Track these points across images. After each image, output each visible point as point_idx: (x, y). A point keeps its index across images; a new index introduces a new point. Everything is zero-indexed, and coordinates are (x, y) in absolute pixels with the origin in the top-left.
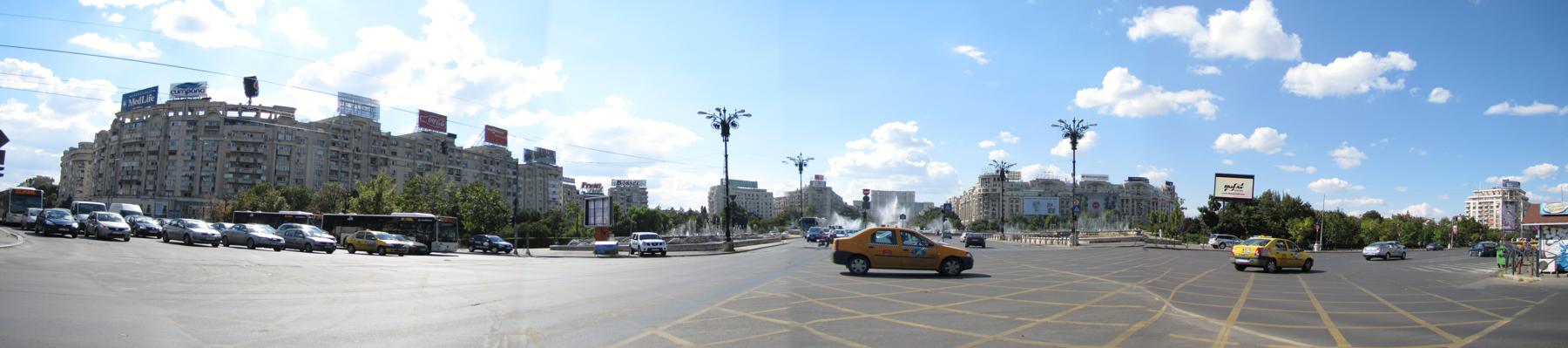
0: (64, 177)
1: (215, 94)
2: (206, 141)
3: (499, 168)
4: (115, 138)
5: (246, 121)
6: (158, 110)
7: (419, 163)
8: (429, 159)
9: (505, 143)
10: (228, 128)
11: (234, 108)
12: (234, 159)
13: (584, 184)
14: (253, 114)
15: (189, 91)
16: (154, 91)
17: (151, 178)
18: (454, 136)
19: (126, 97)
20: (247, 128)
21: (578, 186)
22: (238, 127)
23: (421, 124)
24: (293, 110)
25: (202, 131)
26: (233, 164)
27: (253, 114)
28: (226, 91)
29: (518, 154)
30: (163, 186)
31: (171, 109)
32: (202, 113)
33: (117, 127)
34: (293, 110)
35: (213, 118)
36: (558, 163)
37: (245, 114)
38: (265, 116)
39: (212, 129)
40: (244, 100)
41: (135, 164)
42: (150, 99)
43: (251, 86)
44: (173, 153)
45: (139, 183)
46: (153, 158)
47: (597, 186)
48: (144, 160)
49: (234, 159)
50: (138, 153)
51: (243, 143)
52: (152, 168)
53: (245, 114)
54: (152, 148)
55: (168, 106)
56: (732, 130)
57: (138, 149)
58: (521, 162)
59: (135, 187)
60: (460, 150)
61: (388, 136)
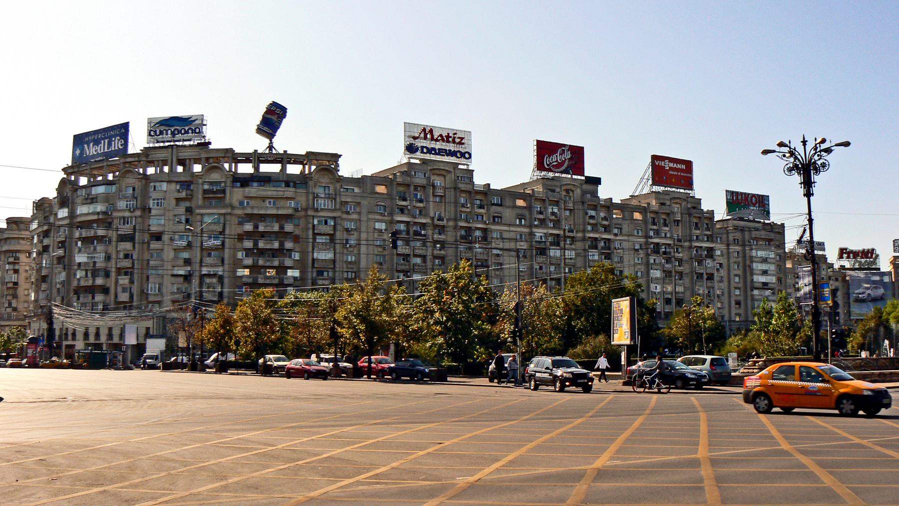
0: (614, 345)
1: (218, 137)
2: (209, 217)
3: (679, 232)
4: (63, 213)
5: (267, 179)
6: (129, 163)
7: (539, 233)
8: (557, 224)
9: (689, 184)
10: (237, 195)
11: (247, 158)
12: (248, 244)
13: (843, 252)
14: (275, 168)
15: (176, 126)
16: (123, 130)
17: (124, 280)
18: (597, 181)
19: (80, 140)
20: (269, 191)
21: (832, 255)
22: (254, 190)
23: (540, 166)
24: (336, 157)
25: (199, 199)
26: (248, 252)
27: (275, 168)
28: (232, 130)
29: (714, 203)
30: (144, 294)
31: (151, 163)
32: (197, 168)
33: (67, 191)
34: (336, 157)
35: (215, 176)
36: (775, 218)
37: (265, 168)
38: (294, 169)
39: (215, 195)
40: (261, 144)
41: (100, 258)
42: (117, 144)
43: (272, 119)
44: (158, 237)
45: (105, 290)
46: (127, 246)
47: (869, 254)
48: (112, 249)
49: (248, 244)
50: (101, 239)
51: (263, 217)
52: (127, 263)
53: (265, 168)
54: (126, 229)
55: (146, 156)
56: (815, 178)
57: (101, 232)
58: (721, 213)
59: (99, 298)
60: (609, 205)
61: (487, 191)
